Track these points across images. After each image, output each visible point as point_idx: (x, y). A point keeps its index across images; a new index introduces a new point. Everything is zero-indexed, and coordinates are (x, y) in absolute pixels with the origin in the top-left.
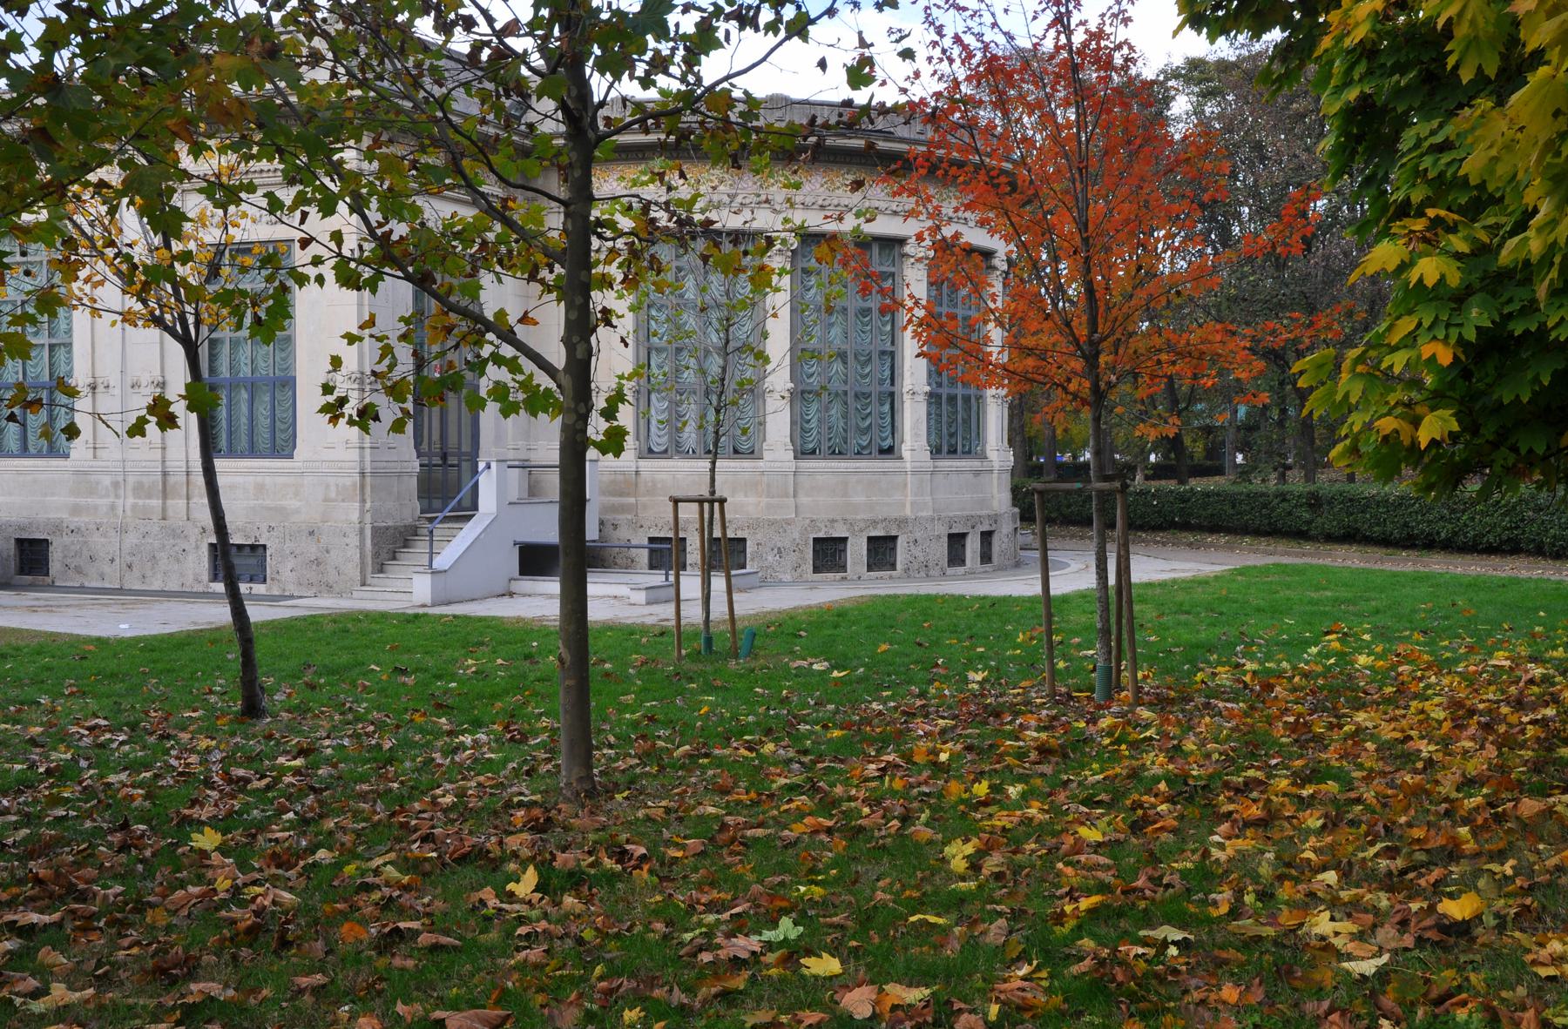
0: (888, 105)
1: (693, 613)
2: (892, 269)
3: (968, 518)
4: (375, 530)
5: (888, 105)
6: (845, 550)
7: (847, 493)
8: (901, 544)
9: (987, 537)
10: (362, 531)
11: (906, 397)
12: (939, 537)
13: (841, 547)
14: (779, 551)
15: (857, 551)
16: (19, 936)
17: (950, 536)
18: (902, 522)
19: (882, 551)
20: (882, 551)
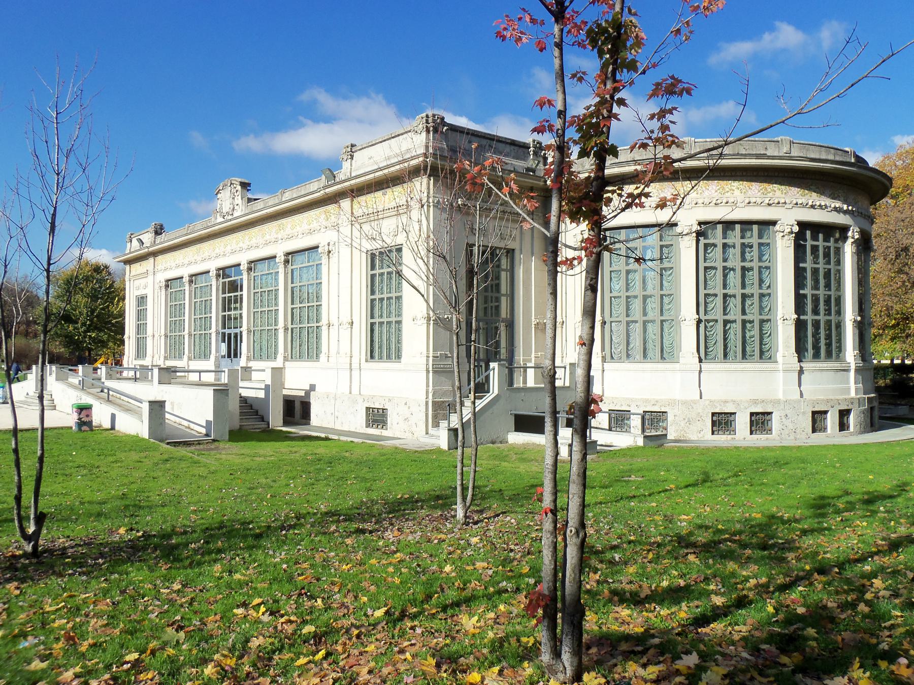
0: (252, 136)
1: (28, 419)
2: (768, 241)
3: (828, 401)
4: (434, 403)
5: (252, 136)
6: (771, 420)
7: (737, 385)
8: (775, 418)
9: (844, 414)
10: (427, 403)
11: (780, 322)
12: (804, 413)
13: (768, 417)
14: (689, 421)
15: (742, 422)
16: (678, 670)
17: (814, 413)
18: (777, 402)
19: (759, 421)
20: (759, 421)
